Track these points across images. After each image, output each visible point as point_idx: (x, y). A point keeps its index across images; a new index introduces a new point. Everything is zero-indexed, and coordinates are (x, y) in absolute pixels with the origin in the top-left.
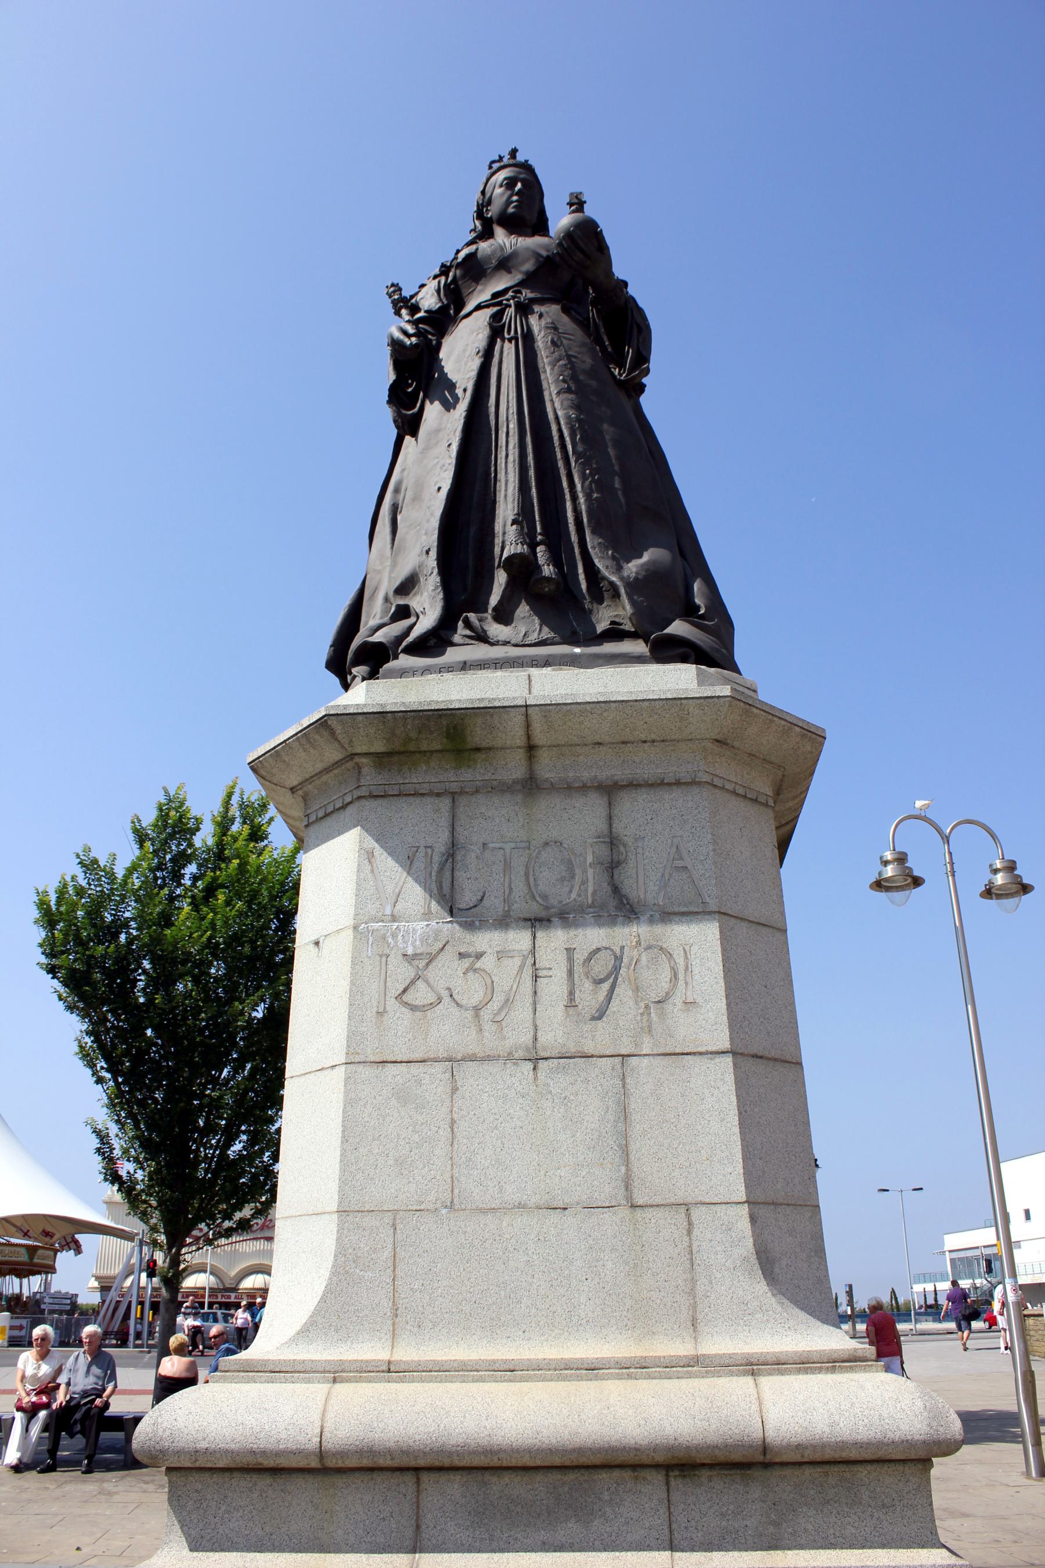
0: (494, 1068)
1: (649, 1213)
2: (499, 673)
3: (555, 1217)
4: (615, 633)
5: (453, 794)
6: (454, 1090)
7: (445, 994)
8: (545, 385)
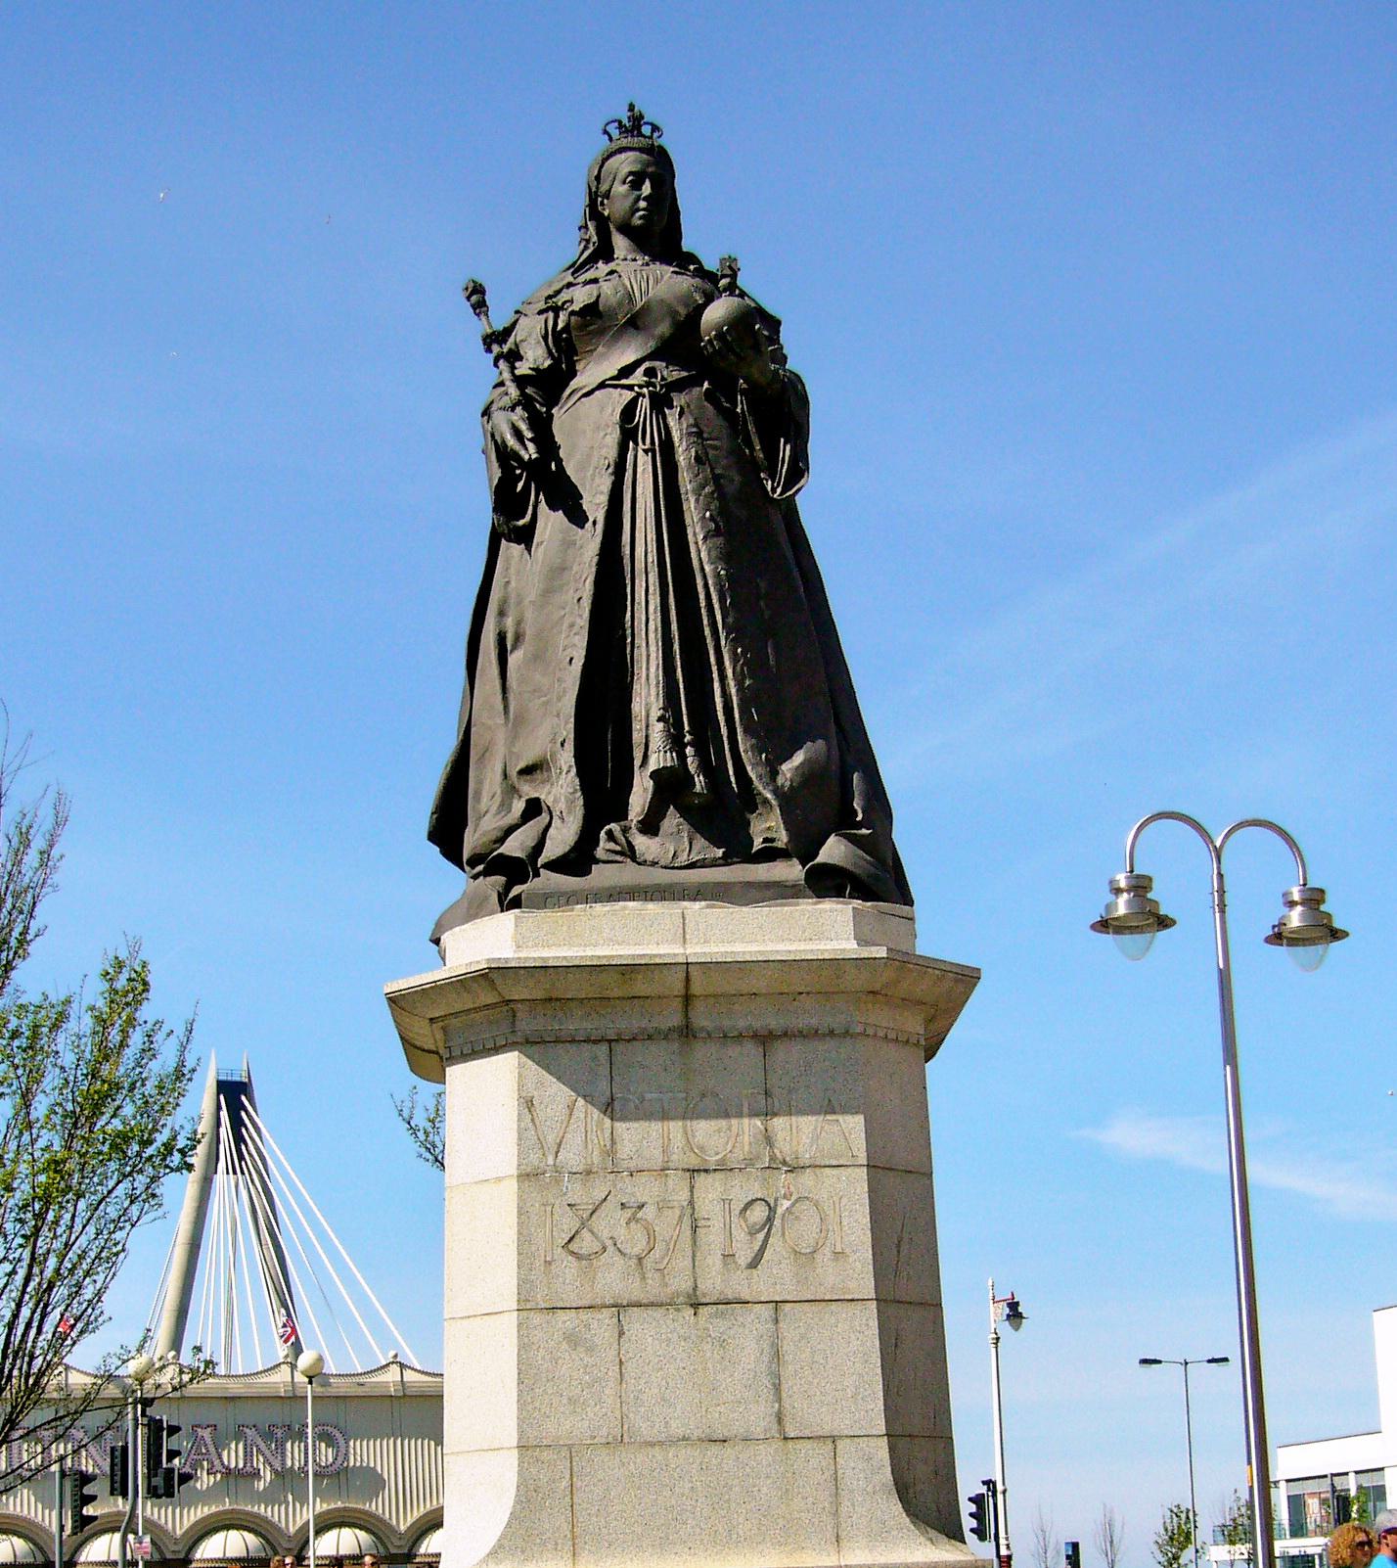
0: (658, 1313)
1: (800, 1444)
2: (652, 907)
3: (715, 1448)
4: (770, 854)
5: (610, 1041)
6: (621, 1334)
7: (609, 1243)
8: (688, 521)
